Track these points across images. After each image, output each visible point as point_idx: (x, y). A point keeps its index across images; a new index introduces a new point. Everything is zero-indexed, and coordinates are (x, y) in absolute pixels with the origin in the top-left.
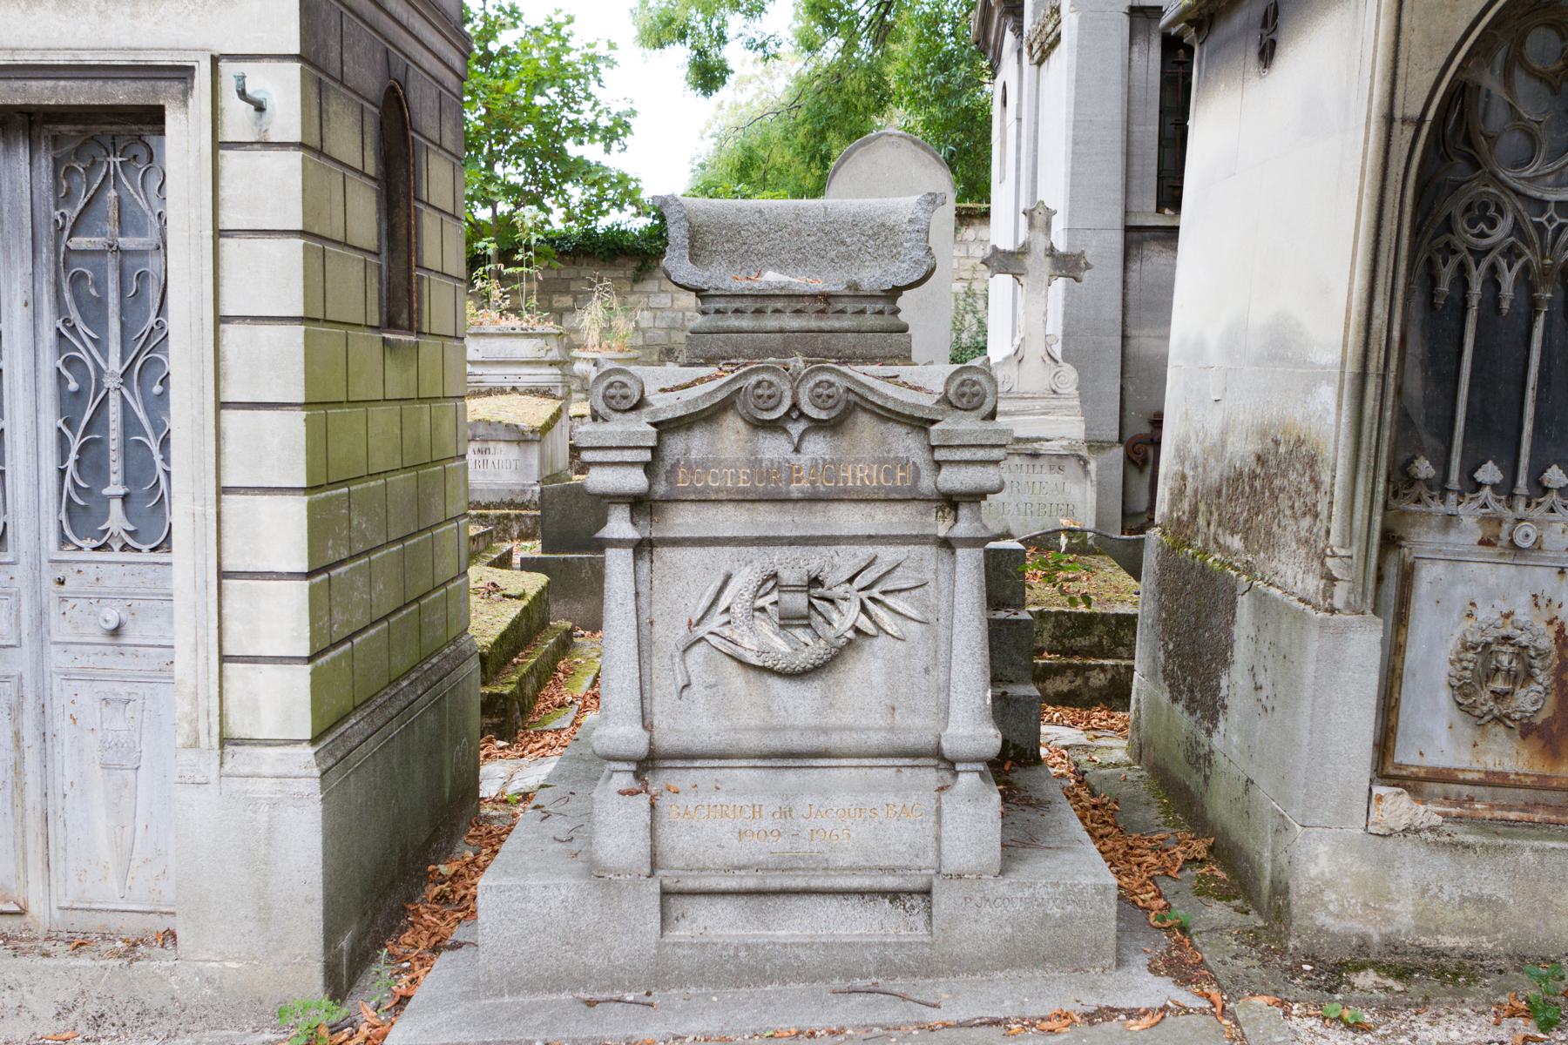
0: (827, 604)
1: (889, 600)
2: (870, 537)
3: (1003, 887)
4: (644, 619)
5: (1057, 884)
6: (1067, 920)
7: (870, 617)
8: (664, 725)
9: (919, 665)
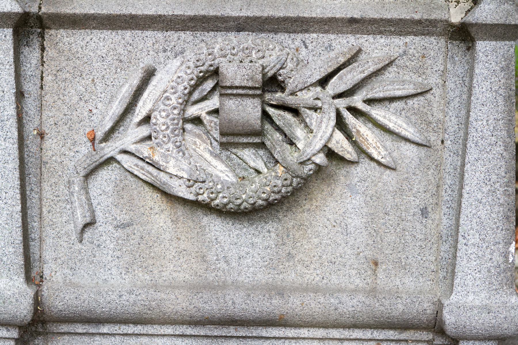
0: (289, 116)
1: (377, 113)
2: (352, 21)
4: (31, 130)
7: (349, 136)
8: (58, 278)
9: (415, 203)
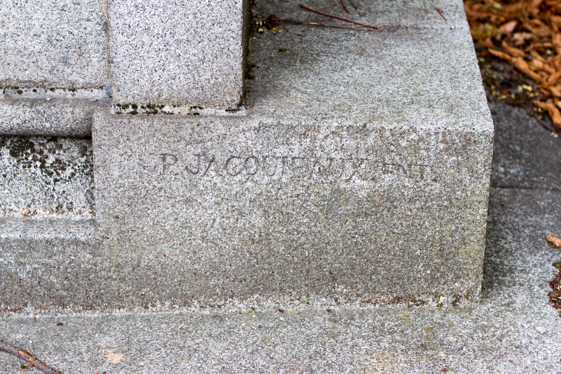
3: (245, 132)
5: (363, 130)
6: (381, 205)
